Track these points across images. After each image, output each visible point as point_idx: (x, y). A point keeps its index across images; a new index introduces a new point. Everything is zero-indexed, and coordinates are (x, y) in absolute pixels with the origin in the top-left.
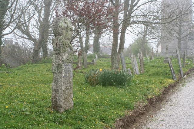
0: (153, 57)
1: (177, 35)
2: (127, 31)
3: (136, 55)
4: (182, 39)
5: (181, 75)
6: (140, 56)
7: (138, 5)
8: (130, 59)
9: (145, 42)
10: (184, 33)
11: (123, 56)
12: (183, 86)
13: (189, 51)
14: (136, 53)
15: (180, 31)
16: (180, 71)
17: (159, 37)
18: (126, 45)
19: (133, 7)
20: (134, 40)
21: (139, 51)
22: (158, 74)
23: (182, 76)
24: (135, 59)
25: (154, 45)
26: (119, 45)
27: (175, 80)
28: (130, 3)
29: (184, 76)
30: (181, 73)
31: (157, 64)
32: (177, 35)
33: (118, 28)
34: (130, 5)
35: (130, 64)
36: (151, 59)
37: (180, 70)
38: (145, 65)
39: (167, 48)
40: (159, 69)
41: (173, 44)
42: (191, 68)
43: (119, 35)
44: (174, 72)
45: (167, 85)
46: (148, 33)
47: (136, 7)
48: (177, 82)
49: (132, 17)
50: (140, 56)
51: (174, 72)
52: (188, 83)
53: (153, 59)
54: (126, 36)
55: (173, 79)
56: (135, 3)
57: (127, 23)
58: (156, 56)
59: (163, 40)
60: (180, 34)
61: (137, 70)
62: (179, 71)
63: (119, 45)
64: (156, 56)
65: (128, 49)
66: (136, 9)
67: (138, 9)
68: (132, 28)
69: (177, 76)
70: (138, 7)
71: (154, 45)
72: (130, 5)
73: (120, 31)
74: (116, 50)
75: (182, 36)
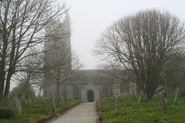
0: (35, 100)
1: (56, 80)
2: (12, 78)
3: (20, 99)
4: (60, 84)
5: (54, 113)
6: (23, 98)
7: (22, 56)
8: (14, 102)
9: (29, 87)
10: (63, 79)
11: (8, 98)
12: (54, 120)
13: (68, 94)
14: (19, 96)
15: (59, 76)
16: (54, 110)
17: (42, 81)
18: (11, 89)
19: (17, 57)
20: (18, 84)
21: (22, 94)
22: (36, 112)
23: (56, 113)
24: (18, 101)
25: (37, 90)
26: (4, 89)
27: (49, 116)
28: (15, 54)
29: (57, 114)
30: (54, 111)
31: (37, 105)
32: (56, 80)
33: (3, 42)
34: (15, 57)
35: (15, 105)
36: (33, 101)
37: (54, 109)
38: (27, 106)
39: (46, 92)
40: (37, 109)
41: (53, 87)
42: (64, 107)
43: (5, 81)
44: (48, 111)
45: (41, 118)
46: (31, 78)
47: (20, 58)
48: (51, 118)
49: (16, 66)
50: (23, 98)
51: (48, 111)
52: (59, 118)
53: (34, 102)
54: (11, 81)
55: (47, 115)
56: (19, 55)
57: (12, 71)
58: (39, 99)
59: (43, 86)
60: (58, 80)
61: (20, 110)
62: (53, 110)
63: (4, 89)
64: (39, 99)
65: (12, 92)
66: (20, 60)
67: (22, 60)
68: (16, 75)
69: (51, 113)
70: (22, 58)
71: (37, 89)
72: (15, 57)
73: (6, 77)
74: (14, 52)
75: (60, 81)
